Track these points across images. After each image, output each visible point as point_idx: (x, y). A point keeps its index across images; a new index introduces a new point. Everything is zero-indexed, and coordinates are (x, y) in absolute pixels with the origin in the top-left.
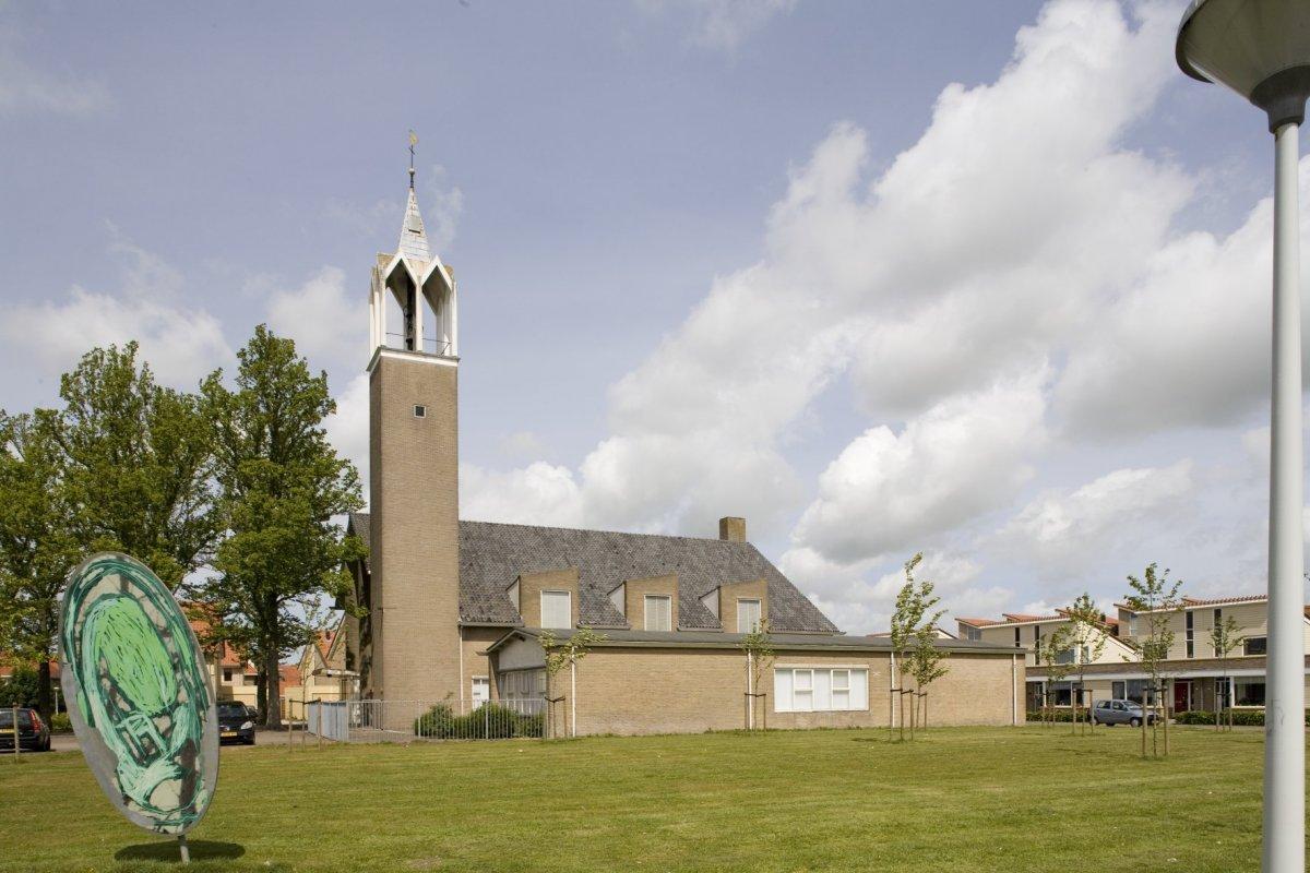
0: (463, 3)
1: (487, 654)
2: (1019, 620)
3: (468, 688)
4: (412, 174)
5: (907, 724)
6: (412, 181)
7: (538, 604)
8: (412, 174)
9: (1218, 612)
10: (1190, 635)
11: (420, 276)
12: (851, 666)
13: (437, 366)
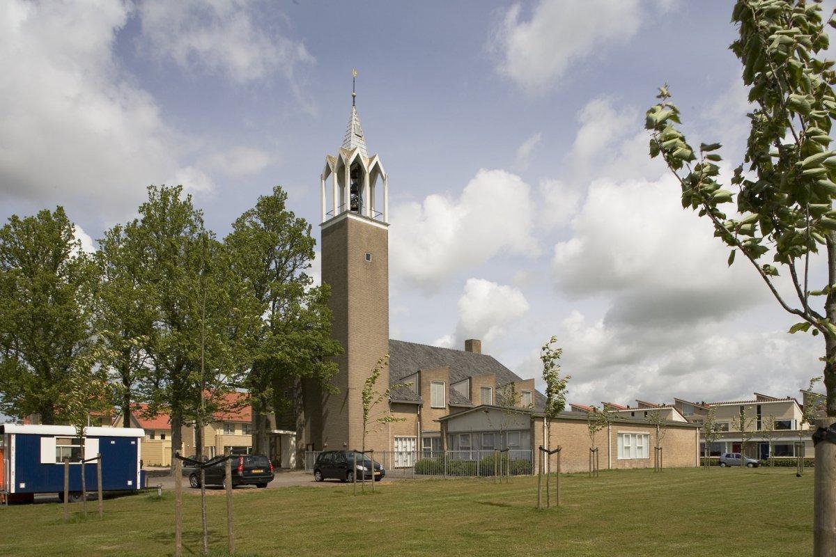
0: (295, 2)
1: (440, 421)
2: (647, 407)
3: (393, 443)
4: (354, 97)
5: (592, 470)
6: (354, 102)
7: (429, 390)
8: (354, 97)
9: (742, 408)
10: (760, 418)
11: (368, 168)
12: (643, 433)
13: (377, 228)
